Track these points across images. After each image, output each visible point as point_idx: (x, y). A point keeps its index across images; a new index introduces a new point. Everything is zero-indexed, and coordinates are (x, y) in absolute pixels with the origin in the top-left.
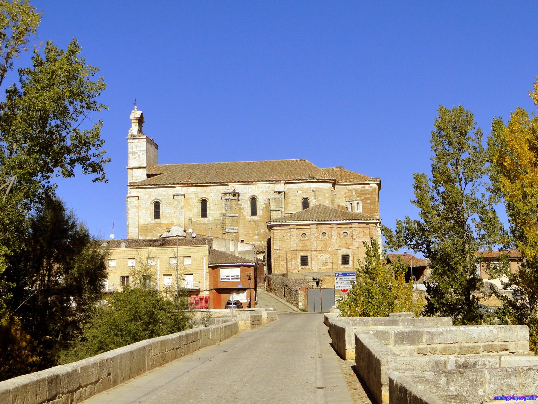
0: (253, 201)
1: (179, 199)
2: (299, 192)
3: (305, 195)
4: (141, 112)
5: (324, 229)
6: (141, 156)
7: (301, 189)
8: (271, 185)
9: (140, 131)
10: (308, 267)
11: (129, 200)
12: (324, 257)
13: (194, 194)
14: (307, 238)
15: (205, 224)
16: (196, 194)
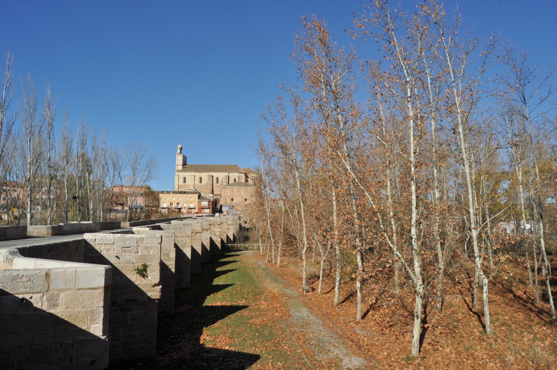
0: (217, 179)
9: (181, 153)
13: (198, 175)
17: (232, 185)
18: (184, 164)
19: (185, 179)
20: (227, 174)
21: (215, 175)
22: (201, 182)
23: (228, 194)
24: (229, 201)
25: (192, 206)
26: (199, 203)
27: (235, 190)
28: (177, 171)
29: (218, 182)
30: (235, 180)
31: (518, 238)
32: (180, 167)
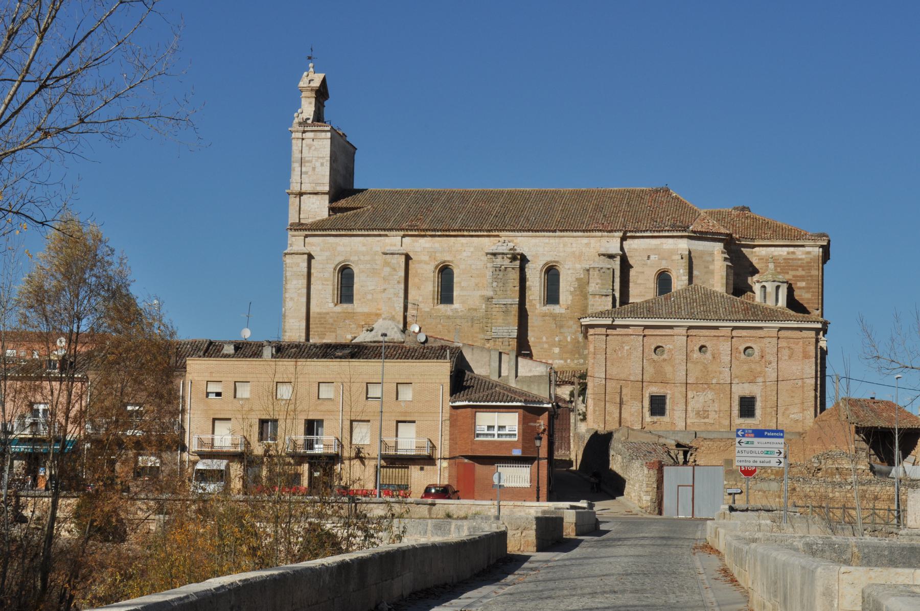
0: (552, 273)
1: (394, 261)
2: (652, 257)
3: (664, 265)
4: (322, 76)
5: (702, 337)
6: (319, 169)
7: (656, 250)
8: (593, 240)
9: (319, 117)
10: (665, 419)
11: (288, 260)
12: (698, 400)
13: (428, 250)
14: (665, 356)
15: (448, 317)
16: (432, 254)
17: (648, 310)
18: (342, 189)
19: (345, 275)
20: (612, 244)
21: (540, 248)
22: (446, 294)
23: (633, 369)
24: (636, 412)
25: (408, 441)
26: (461, 423)
27: (676, 343)
28: (299, 227)
29: (552, 296)
30: (664, 281)
31: (300, 539)
32: (317, 208)
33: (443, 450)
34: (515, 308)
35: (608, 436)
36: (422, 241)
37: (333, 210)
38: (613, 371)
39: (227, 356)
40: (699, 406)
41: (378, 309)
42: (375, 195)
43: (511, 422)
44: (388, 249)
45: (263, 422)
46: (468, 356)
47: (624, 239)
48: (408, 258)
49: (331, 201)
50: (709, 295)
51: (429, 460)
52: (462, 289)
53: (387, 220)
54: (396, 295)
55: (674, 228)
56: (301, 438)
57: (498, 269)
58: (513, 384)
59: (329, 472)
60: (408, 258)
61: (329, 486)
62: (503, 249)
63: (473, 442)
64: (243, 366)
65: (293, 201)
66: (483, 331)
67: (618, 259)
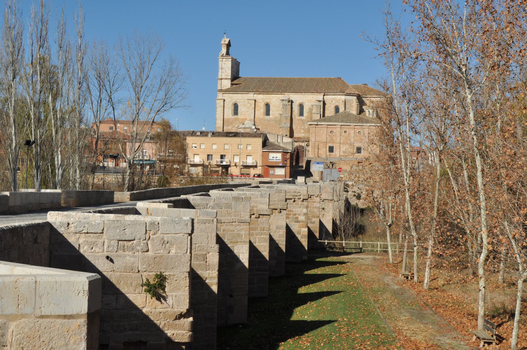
0: (301, 106)
3: (337, 104)
4: (228, 39)
5: (345, 128)
6: (227, 71)
7: (334, 99)
8: (314, 96)
9: (228, 53)
10: (333, 154)
11: (217, 101)
12: (344, 148)
13: (262, 98)
16: (263, 100)
17: (330, 119)
18: (235, 77)
20: (320, 97)
21: (297, 98)
22: (268, 113)
24: (324, 152)
25: (250, 161)
26: (265, 156)
27: (337, 130)
28: (221, 91)
29: (301, 114)
30: (337, 109)
32: (227, 84)
33: (260, 163)
34: (289, 117)
35: (310, 161)
36: (260, 95)
37: (232, 84)
38: (318, 139)
39: (198, 136)
40: (344, 150)
41: (246, 119)
42: (246, 79)
43: (279, 156)
44: (249, 98)
45: (208, 155)
46: (268, 136)
47: (324, 95)
48: (255, 101)
49: (232, 81)
50: (349, 114)
51: (256, 166)
52: (273, 111)
53: (249, 88)
54: (252, 113)
55: (341, 92)
56: (219, 160)
57: (284, 105)
58: (281, 145)
59: (227, 170)
60: (255, 101)
61: (227, 173)
62: (286, 99)
63: (268, 162)
64: (203, 139)
65: (219, 81)
66: (279, 125)
67: (322, 102)
